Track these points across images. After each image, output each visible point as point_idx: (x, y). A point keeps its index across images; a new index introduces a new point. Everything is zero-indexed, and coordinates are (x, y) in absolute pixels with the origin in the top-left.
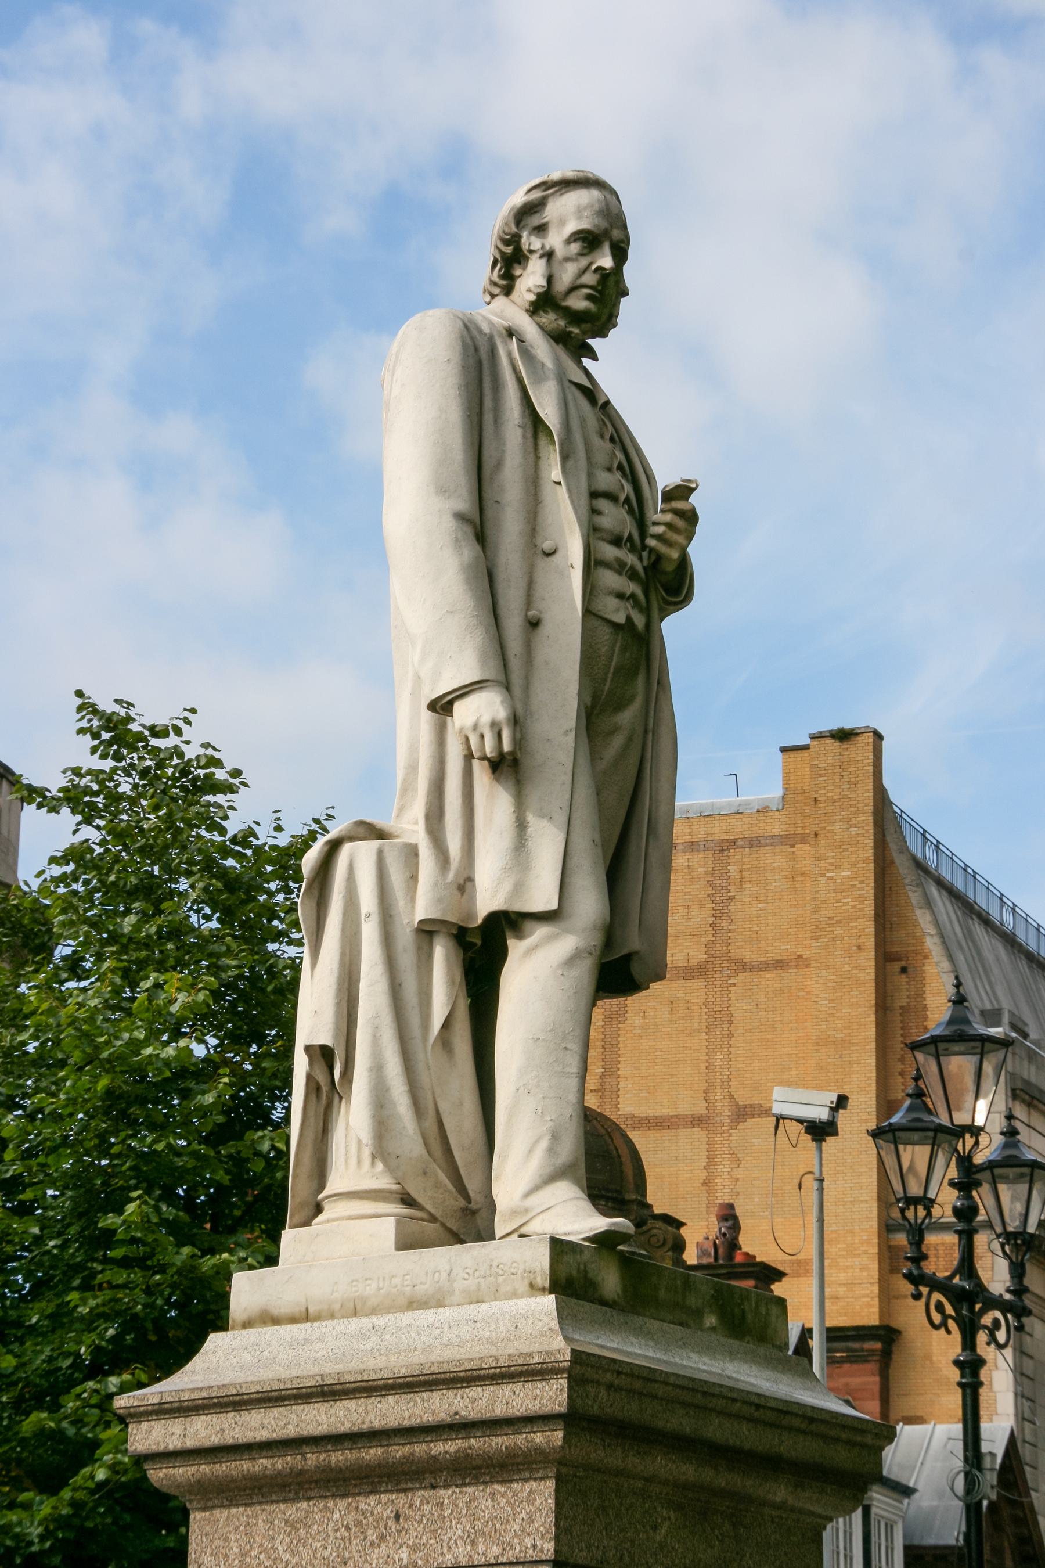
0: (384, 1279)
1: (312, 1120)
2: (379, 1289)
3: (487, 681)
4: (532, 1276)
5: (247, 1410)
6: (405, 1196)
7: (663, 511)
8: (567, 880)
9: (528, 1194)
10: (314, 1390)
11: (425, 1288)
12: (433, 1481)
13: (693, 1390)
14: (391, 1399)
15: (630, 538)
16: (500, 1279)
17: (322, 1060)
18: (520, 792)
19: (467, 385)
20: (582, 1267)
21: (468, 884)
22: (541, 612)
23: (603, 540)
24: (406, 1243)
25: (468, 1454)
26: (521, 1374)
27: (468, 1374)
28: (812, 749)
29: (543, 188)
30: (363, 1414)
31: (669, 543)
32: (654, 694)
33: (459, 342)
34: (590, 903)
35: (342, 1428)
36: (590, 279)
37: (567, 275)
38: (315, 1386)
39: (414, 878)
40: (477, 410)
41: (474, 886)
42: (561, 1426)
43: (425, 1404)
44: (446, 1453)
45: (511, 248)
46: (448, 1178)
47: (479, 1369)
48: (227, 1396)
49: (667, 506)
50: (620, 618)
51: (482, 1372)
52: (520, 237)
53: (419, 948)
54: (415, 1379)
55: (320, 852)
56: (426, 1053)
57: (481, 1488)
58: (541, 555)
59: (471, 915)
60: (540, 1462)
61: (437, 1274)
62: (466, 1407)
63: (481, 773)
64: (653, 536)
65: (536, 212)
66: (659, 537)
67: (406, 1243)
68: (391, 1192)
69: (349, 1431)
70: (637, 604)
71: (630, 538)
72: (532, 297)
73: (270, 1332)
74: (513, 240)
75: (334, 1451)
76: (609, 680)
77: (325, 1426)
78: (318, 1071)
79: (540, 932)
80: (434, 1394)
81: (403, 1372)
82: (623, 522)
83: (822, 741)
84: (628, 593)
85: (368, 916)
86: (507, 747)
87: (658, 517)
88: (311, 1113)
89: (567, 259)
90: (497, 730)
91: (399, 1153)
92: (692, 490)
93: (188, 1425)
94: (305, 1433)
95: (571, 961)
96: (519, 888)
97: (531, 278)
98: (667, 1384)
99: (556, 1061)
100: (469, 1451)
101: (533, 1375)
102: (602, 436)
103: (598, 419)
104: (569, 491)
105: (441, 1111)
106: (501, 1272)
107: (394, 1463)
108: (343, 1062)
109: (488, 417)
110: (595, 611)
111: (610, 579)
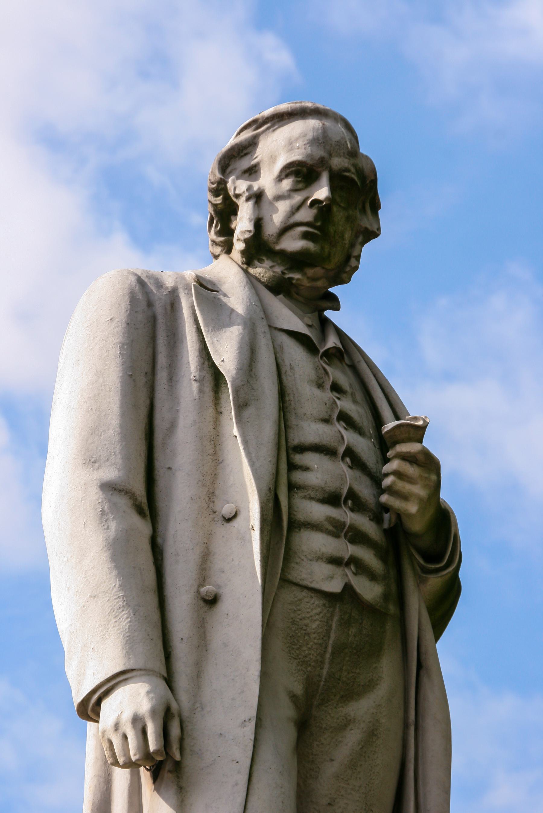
3: (132, 670)
15: (352, 494)
18: (182, 801)
22: (219, 587)
23: (311, 498)
29: (254, 127)
33: (127, 298)
36: (306, 215)
37: (278, 216)
45: (221, 197)
52: (226, 183)
65: (246, 154)
74: (220, 189)
76: (327, 661)
82: (342, 477)
84: (347, 557)
89: (278, 198)
90: (140, 727)
92: (422, 429)
97: (243, 224)
103: (316, 369)
109: (162, 376)
110: (297, 581)
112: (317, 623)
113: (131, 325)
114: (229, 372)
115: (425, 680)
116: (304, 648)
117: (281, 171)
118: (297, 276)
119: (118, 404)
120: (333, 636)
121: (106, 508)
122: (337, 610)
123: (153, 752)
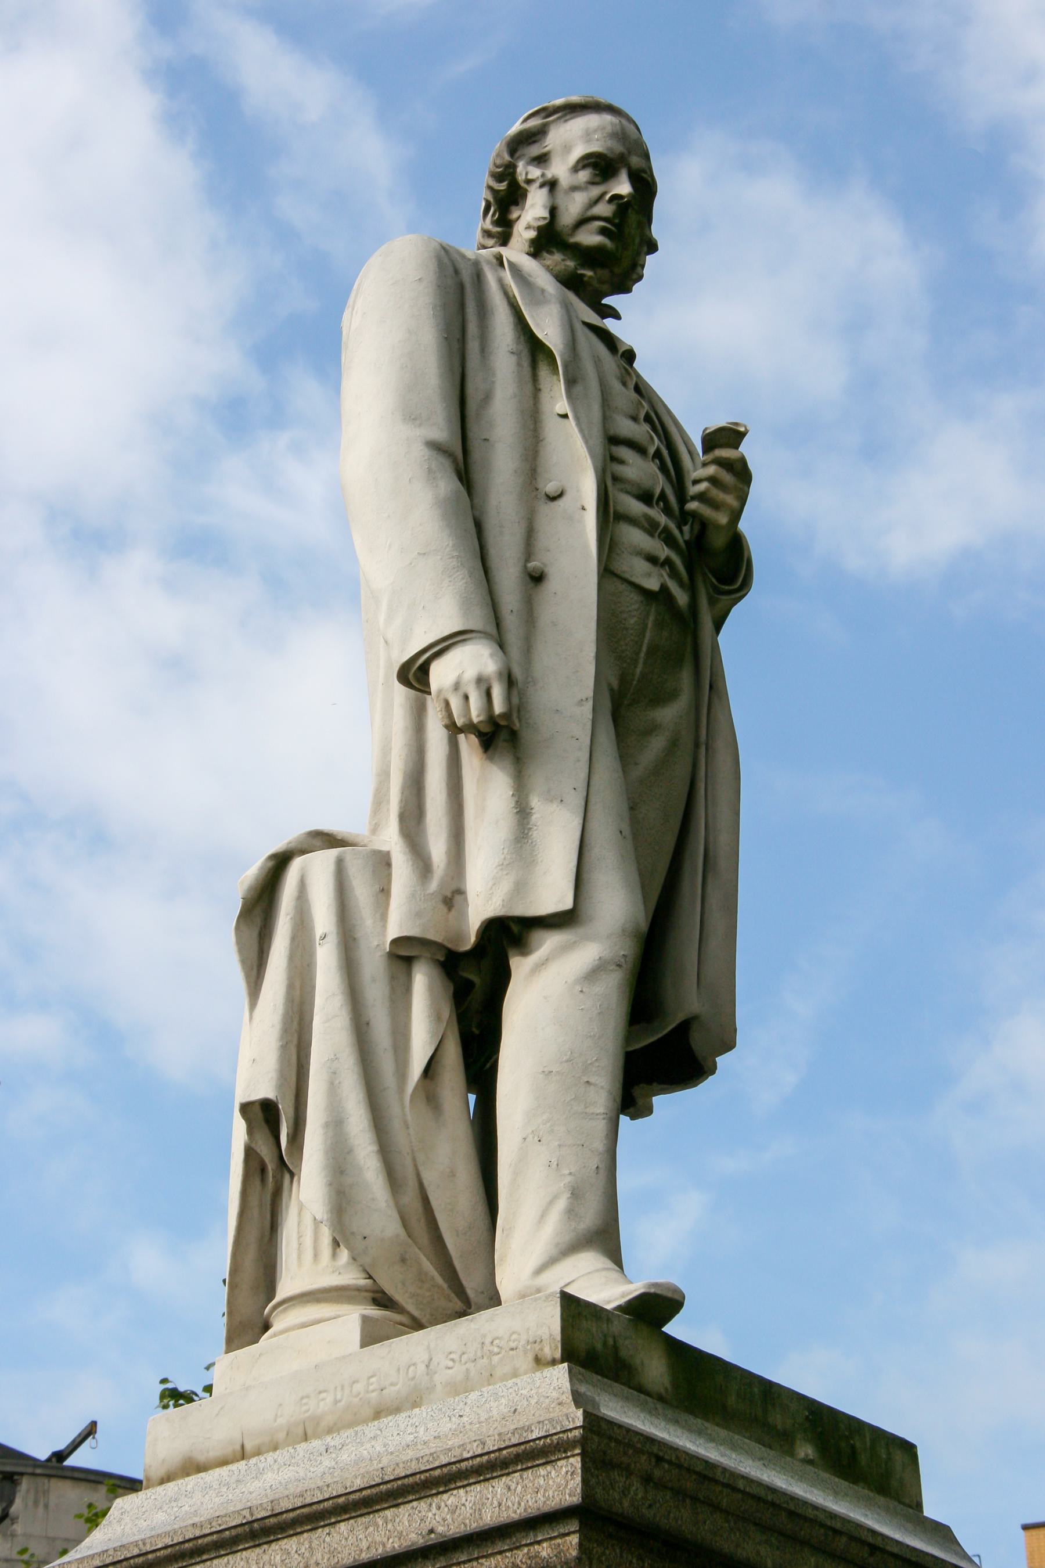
0: (343, 1387)
1: (255, 1212)
2: (336, 1402)
3: (472, 631)
4: (537, 1347)
6: (377, 1295)
7: (705, 465)
8: (585, 876)
10: (240, 1530)
11: (397, 1389)
13: (773, 1504)
14: (343, 1527)
15: (663, 496)
16: (496, 1359)
19: (444, 306)
20: (611, 1341)
21: (457, 898)
22: (545, 565)
23: (628, 493)
24: (372, 1335)
26: (518, 1459)
29: (543, 115)
30: (307, 1554)
31: (716, 505)
34: (616, 905)
36: (604, 209)
37: (573, 207)
38: (242, 1525)
39: (384, 891)
41: (466, 900)
42: (574, 1525)
43: (390, 1526)
45: (505, 183)
46: (436, 1269)
49: (710, 457)
50: (653, 584)
51: (464, 1465)
53: (393, 978)
54: (374, 1491)
55: (261, 868)
56: (401, 1100)
59: (460, 936)
61: (412, 1368)
62: (444, 1520)
64: (693, 498)
65: (534, 142)
66: (701, 497)
67: (371, 1336)
68: (358, 1289)
70: (674, 574)
71: (663, 496)
72: (532, 234)
73: (191, 1482)
74: (506, 173)
78: (260, 1142)
79: (548, 942)
80: (402, 1509)
81: (358, 1483)
84: (663, 557)
85: (324, 937)
86: (498, 707)
88: (254, 1201)
89: (574, 188)
90: (484, 687)
91: (366, 1233)
92: (741, 435)
95: (593, 974)
96: (521, 888)
97: (533, 210)
98: (735, 1489)
99: (576, 1098)
102: (624, 384)
105: (426, 1183)
106: (496, 1350)
108: (291, 1121)
109: (473, 346)
110: (619, 572)
111: (635, 537)
112: (635, 619)
113: (441, 287)
114: (555, 345)
116: (622, 643)
117: (579, 161)
118: (589, 273)
120: (648, 634)
121: (433, 466)
122: (653, 610)
123: (499, 715)
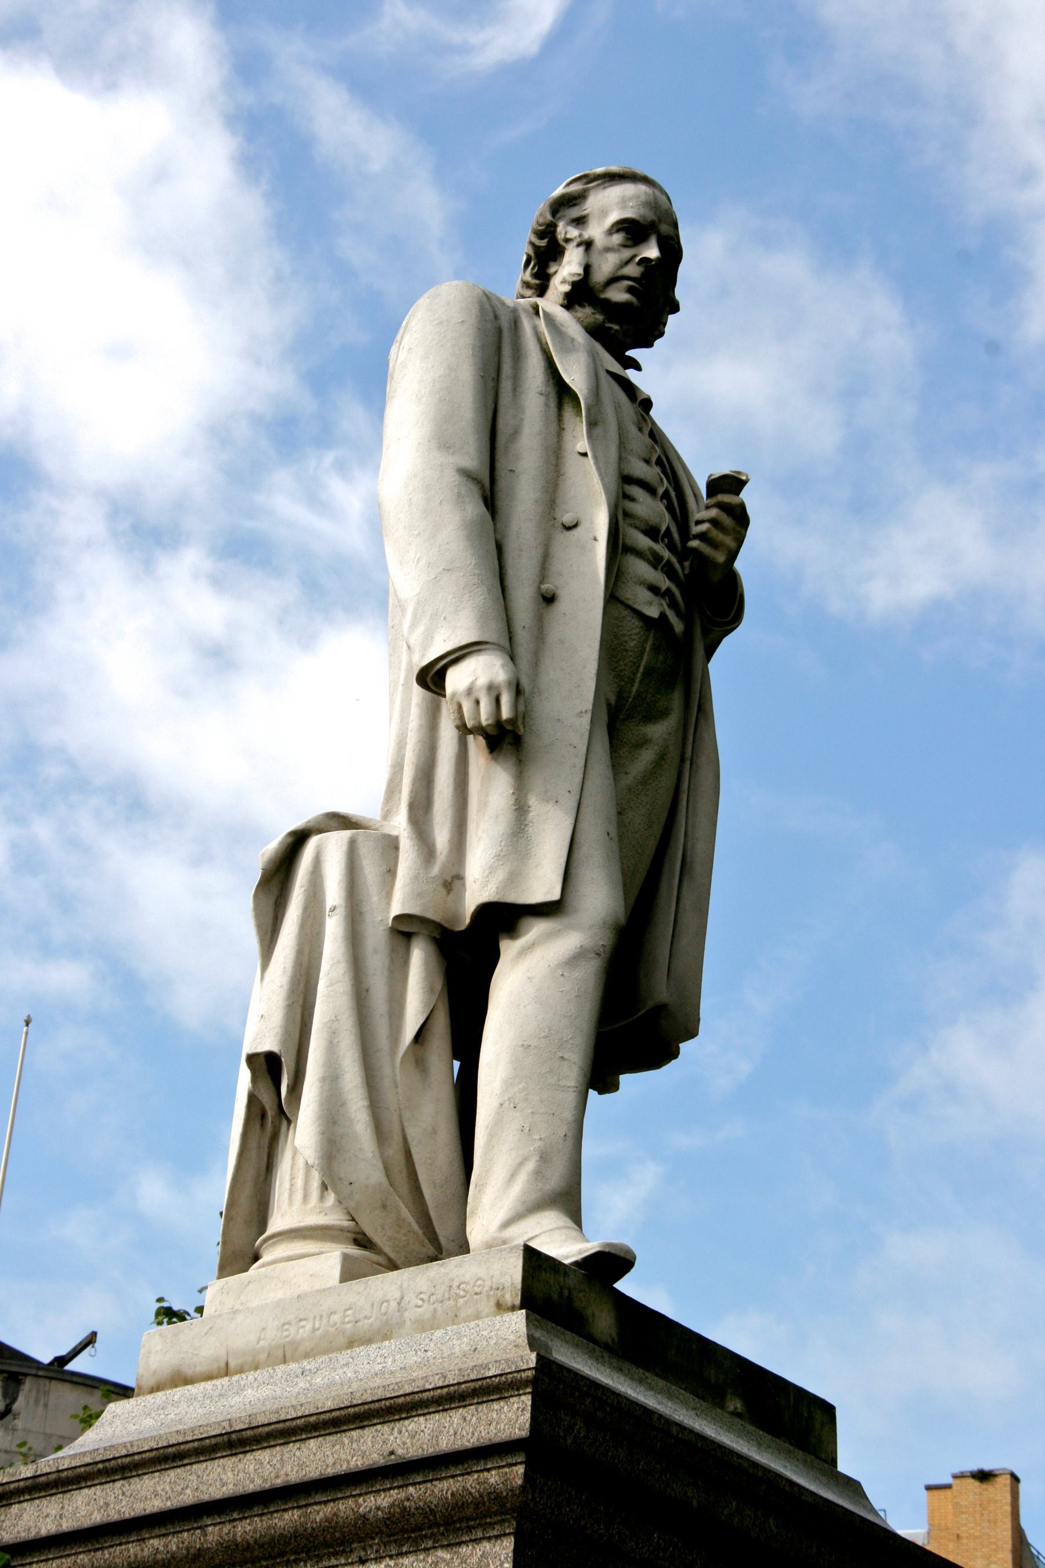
0: (321, 1317)
1: (253, 1154)
2: (314, 1330)
3: (487, 643)
4: (499, 1293)
5: (138, 1475)
6: (359, 1237)
8: (573, 871)
9: (506, 1224)
10: (219, 1439)
12: (362, 1553)
14: (312, 1443)
16: (461, 1301)
17: (268, 1077)
18: (521, 773)
19: (483, 347)
20: (566, 1293)
21: (457, 883)
23: (636, 528)
24: (350, 1273)
25: (405, 1508)
27: (408, 1399)
28: (955, 1488)
30: (278, 1466)
32: (694, 719)
34: (599, 900)
35: (251, 1486)
37: (606, 266)
38: (221, 1435)
39: (391, 872)
40: (494, 375)
41: (464, 885)
43: (355, 1446)
44: (378, 1508)
45: (546, 240)
47: (422, 1392)
48: (115, 1458)
49: (713, 501)
50: (653, 612)
51: (425, 1395)
52: (555, 226)
53: (393, 950)
55: (281, 843)
56: (394, 1068)
57: (421, 1557)
58: (560, 528)
60: (495, 1514)
61: (385, 1304)
62: (404, 1443)
63: (476, 746)
65: (575, 205)
66: (702, 537)
68: (341, 1229)
69: (259, 1489)
70: (673, 604)
72: (567, 288)
74: (547, 232)
75: (240, 1519)
76: (638, 680)
77: (231, 1486)
78: (262, 1090)
79: (536, 929)
80: (367, 1431)
81: (329, 1405)
83: (963, 1480)
84: (664, 588)
86: (506, 713)
87: (698, 516)
88: (253, 1144)
89: (608, 249)
91: (353, 1179)
93: (66, 1502)
94: (206, 1497)
95: (574, 960)
96: (514, 878)
97: (568, 269)
99: (550, 1071)
100: (407, 1504)
101: (489, 1394)
102: (640, 429)
104: (596, 463)
105: (410, 1138)
106: (462, 1293)
107: (313, 1529)
108: (292, 1073)
109: (506, 385)
113: (481, 330)
115: (702, 721)
116: (621, 663)
119: (471, 400)
120: (645, 657)
121: (462, 491)
123: (506, 721)
